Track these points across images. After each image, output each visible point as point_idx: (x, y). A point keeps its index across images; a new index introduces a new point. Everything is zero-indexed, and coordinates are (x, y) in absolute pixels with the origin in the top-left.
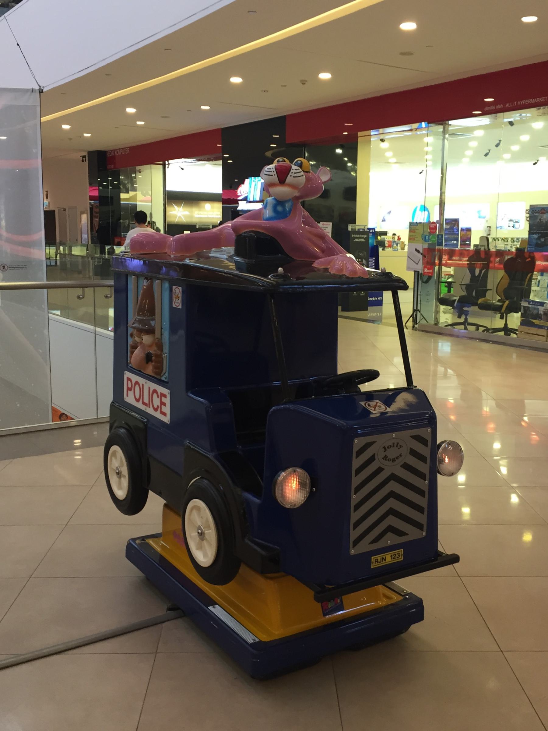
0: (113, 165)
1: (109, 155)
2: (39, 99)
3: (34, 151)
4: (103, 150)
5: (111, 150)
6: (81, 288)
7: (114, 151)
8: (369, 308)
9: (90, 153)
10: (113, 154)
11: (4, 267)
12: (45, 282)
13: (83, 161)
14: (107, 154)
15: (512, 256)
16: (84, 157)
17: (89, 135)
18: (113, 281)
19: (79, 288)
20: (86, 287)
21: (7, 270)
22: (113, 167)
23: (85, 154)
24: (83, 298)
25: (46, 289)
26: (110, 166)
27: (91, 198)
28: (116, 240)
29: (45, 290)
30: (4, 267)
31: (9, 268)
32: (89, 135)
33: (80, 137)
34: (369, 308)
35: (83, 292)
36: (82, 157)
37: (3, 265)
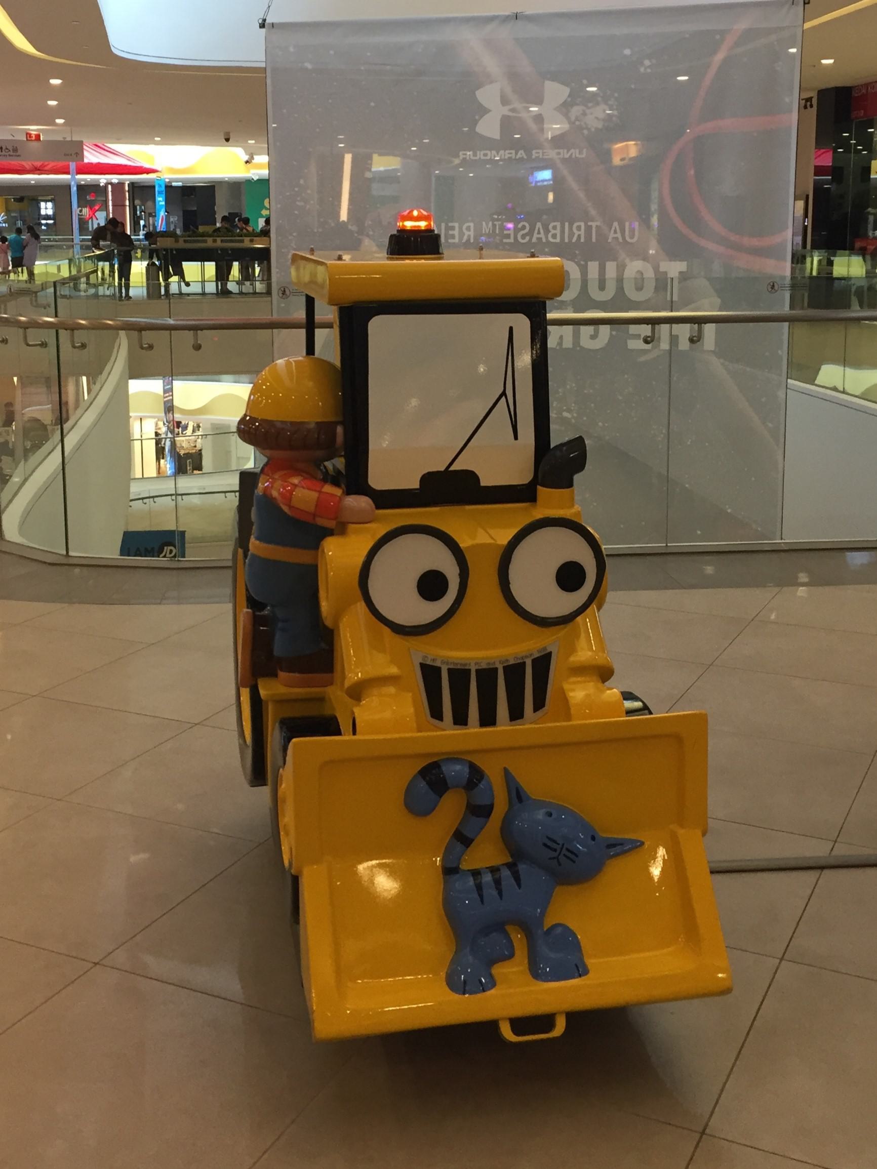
0: (862, 111)
1: (857, 93)
2: (803, 13)
3: (787, 100)
4: (848, 85)
5: (862, 85)
6: (192, 332)
7: (867, 85)
8: (416, 485)
9: (822, 93)
10: (864, 91)
11: (773, 287)
12: (786, 309)
13: (805, 107)
14: (853, 92)
15: (558, 298)
16: (809, 100)
17: (831, 61)
18: (315, 319)
19: (187, 331)
20: (199, 330)
21: (777, 291)
22: (862, 115)
23: (814, 94)
24: (652, 341)
25: (668, 325)
26: (856, 112)
27: (819, 171)
28: (858, 245)
29: (786, 324)
30: (773, 286)
31: (780, 289)
32: (831, 61)
33: (815, 66)
34: (416, 485)
35: (653, 330)
36: (804, 101)
37: (772, 284)
